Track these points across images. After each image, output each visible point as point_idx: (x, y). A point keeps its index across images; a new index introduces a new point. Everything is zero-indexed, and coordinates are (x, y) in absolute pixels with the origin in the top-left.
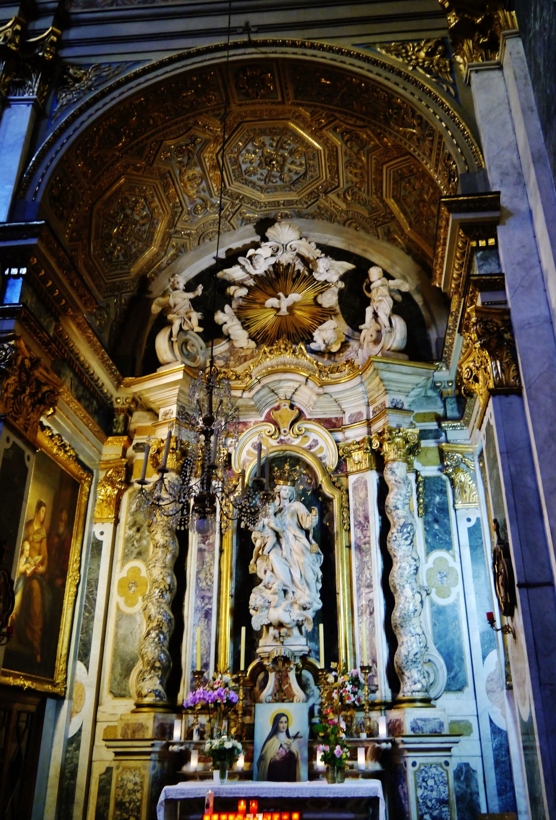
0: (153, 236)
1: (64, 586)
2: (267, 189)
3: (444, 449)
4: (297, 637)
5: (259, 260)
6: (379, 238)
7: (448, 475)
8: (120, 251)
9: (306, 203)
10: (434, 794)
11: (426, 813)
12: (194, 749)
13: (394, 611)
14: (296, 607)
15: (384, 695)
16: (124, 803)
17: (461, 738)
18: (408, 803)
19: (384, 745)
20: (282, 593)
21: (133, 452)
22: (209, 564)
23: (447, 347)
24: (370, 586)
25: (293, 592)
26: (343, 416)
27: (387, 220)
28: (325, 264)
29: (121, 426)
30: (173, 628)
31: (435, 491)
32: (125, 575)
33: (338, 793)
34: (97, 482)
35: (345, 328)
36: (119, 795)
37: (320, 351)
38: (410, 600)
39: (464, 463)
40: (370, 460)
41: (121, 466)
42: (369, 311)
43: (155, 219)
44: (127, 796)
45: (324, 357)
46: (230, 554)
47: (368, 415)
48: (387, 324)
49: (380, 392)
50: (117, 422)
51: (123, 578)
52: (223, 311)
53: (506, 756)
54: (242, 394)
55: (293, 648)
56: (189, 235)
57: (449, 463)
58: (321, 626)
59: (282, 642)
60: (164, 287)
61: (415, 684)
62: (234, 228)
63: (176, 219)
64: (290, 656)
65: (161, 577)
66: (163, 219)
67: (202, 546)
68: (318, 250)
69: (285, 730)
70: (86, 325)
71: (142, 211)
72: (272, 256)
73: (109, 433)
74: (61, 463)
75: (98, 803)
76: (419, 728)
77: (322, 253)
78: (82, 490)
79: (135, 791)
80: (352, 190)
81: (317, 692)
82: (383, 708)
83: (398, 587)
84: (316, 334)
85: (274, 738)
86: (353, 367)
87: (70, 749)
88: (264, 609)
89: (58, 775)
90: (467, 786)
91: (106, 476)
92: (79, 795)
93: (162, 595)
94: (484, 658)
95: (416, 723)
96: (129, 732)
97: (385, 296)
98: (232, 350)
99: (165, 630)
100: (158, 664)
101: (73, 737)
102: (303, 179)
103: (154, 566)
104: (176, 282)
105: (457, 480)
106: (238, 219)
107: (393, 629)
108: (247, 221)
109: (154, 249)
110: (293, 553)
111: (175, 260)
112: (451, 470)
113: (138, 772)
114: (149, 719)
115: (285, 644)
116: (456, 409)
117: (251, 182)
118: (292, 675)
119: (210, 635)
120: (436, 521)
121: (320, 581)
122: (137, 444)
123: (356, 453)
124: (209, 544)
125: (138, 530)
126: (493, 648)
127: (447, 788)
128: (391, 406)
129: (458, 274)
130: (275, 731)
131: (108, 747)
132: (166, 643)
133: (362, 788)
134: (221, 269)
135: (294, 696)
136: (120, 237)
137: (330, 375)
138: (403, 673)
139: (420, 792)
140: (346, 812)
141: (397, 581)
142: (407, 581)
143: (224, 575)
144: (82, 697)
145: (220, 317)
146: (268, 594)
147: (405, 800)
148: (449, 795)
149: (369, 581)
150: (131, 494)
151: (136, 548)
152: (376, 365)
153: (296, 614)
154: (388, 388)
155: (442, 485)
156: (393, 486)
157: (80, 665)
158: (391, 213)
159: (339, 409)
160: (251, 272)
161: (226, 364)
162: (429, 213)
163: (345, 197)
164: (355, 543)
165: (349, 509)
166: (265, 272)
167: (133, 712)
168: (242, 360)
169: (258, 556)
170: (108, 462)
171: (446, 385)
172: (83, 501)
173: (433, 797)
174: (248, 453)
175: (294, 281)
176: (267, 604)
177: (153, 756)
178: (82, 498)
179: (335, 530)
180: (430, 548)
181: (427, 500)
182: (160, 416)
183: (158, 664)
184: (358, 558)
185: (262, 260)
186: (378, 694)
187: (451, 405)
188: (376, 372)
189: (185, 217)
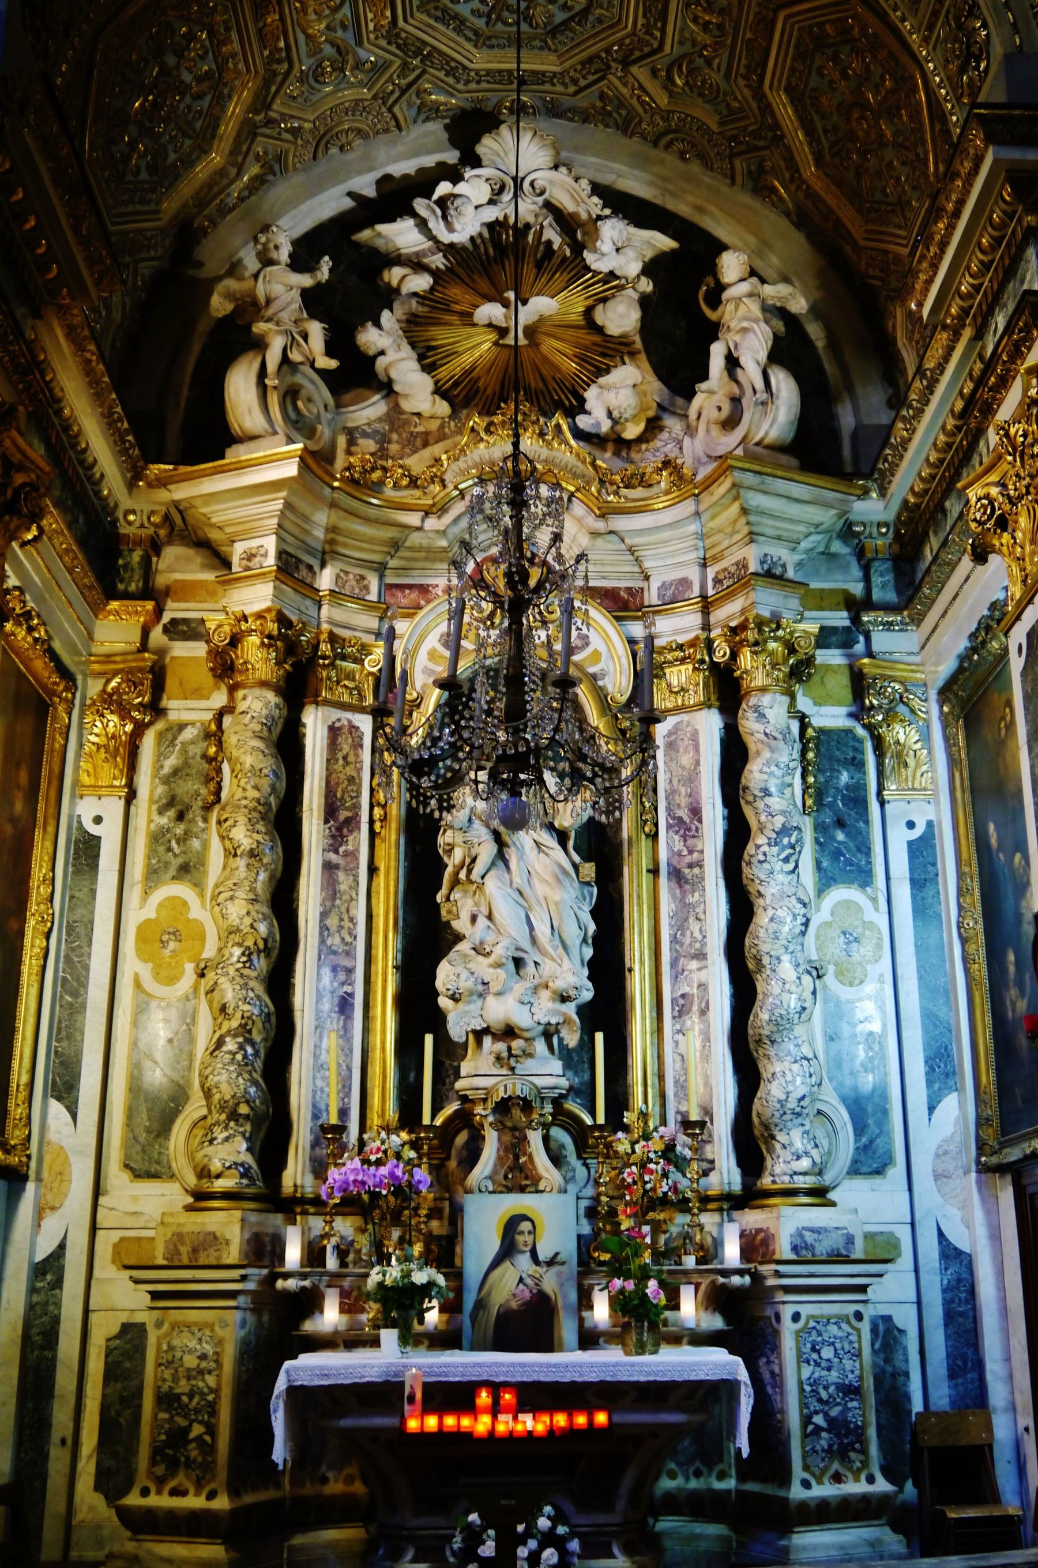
0: (217, 126)
1: (21, 934)
2: (489, 38)
3: (865, 671)
4: (545, 1058)
5: (462, 209)
6: (733, 182)
7: (870, 728)
8: (144, 155)
9: (575, 82)
10: (834, 1376)
11: (817, 1412)
12: (329, 1286)
13: (756, 1008)
14: (545, 995)
15: (726, 1181)
16: (178, 1396)
17: (889, 1266)
18: (782, 1393)
19: (736, 1280)
20: (511, 966)
21: (165, 638)
22: (346, 897)
23: (894, 448)
24: (701, 956)
25: (536, 963)
26: (645, 585)
27: (761, 143)
28: (615, 234)
29: (136, 577)
30: (272, 1034)
31: (838, 761)
32: (153, 916)
33: (655, 1373)
34: (83, 704)
35: (655, 390)
36: (164, 1380)
37: (597, 436)
38: (793, 988)
39: (906, 704)
40: (706, 686)
41: (141, 670)
42: (717, 352)
43: (225, 85)
44: (183, 1382)
45: (604, 450)
46: (392, 876)
47: (703, 586)
48: (759, 384)
49: (737, 537)
50: (126, 566)
51: (148, 921)
52: (378, 325)
53: (967, 1302)
54: (423, 521)
55: (540, 1082)
56: (296, 132)
57: (875, 702)
58: (599, 1037)
59: (513, 1069)
60: (232, 255)
61: (798, 1158)
62: (399, 128)
63: (273, 89)
64: (532, 1098)
65: (248, 921)
66: (244, 86)
67: (332, 856)
68: (595, 199)
69: (528, 1249)
70: (86, 333)
71: (199, 63)
72: (491, 202)
73: (113, 594)
74: (17, 655)
75: (104, 1396)
76: (807, 1247)
77: (604, 206)
78: (54, 720)
79: (201, 1372)
80: (690, 62)
81: (581, 1172)
82: (725, 1207)
83: (766, 960)
84: (591, 395)
85: (507, 1264)
86: (681, 477)
87: (39, 1285)
88: (475, 997)
89: (19, 1341)
90: (887, 1360)
91: (104, 691)
92: (65, 1380)
93: (249, 963)
94: (931, 1109)
95: (801, 1236)
96: (184, 1250)
97: (756, 321)
98: (396, 416)
99: (257, 1037)
100: (244, 1109)
101: (45, 1261)
102: (579, 24)
103: (232, 898)
104: (271, 246)
105: (889, 739)
106: (410, 105)
107: (752, 1046)
108: (432, 112)
109: (216, 158)
110: (535, 880)
111: (257, 189)
112: (880, 718)
113: (208, 1333)
114: (230, 1222)
115: (517, 1072)
116: (891, 585)
117: (456, 17)
118: (535, 1138)
119: (351, 1050)
120: (840, 824)
121: (590, 941)
122: (174, 622)
123: (675, 669)
124: (346, 854)
125: (180, 817)
126: (951, 1090)
127: (857, 1364)
128: (760, 571)
129: (972, 285)
130: (508, 1250)
131: (137, 1282)
132: (259, 1064)
133: (706, 1364)
134: (370, 223)
135: (540, 1179)
136: (147, 124)
137: (624, 491)
138: (773, 1137)
139: (806, 1371)
140: (669, 1410)
141: (764, 948)
142: (786, 949)
143: (379, 923)
144: (63, 1175)
145: (370, 338)
146: (482, 966)
147: (774, 1387)
148: (861, 1378)
149: (698, 945)
150: (160, 735)
151: (176, 855)
152: (737, 474)
153: (546, 1010)
154: (755, 529)
155: (855, 749)
156: (760, 746)
157: (56, 1108)
158: (776, 125)
159: (637, 569)
160: (441, 238)
161: (382, 449)
162: (873, 136)
163: (670, 78)
164: (668, 865)
165: (655, 790)
166: (472, 239)
167: (189, 1208)
168: (419, 442)
169: (455, 882)
170: (108, 658)
171: (875, 530)
172: (57, 745)
173: (831, 1380)
174: (432, 655)
175: (539, 265)
176: (480, 988)
177: (242, 1300)
178: (54, 739)
179: (625, 834)
180: (826, 881)
181: (822, 779)
182: (235, 560)
183: (244, 1109)
184: (674, 897)
185: (469, 210)
186: (713, 1178)
187: (882, 575)
188: (734, 492)
189: (292, 88)
